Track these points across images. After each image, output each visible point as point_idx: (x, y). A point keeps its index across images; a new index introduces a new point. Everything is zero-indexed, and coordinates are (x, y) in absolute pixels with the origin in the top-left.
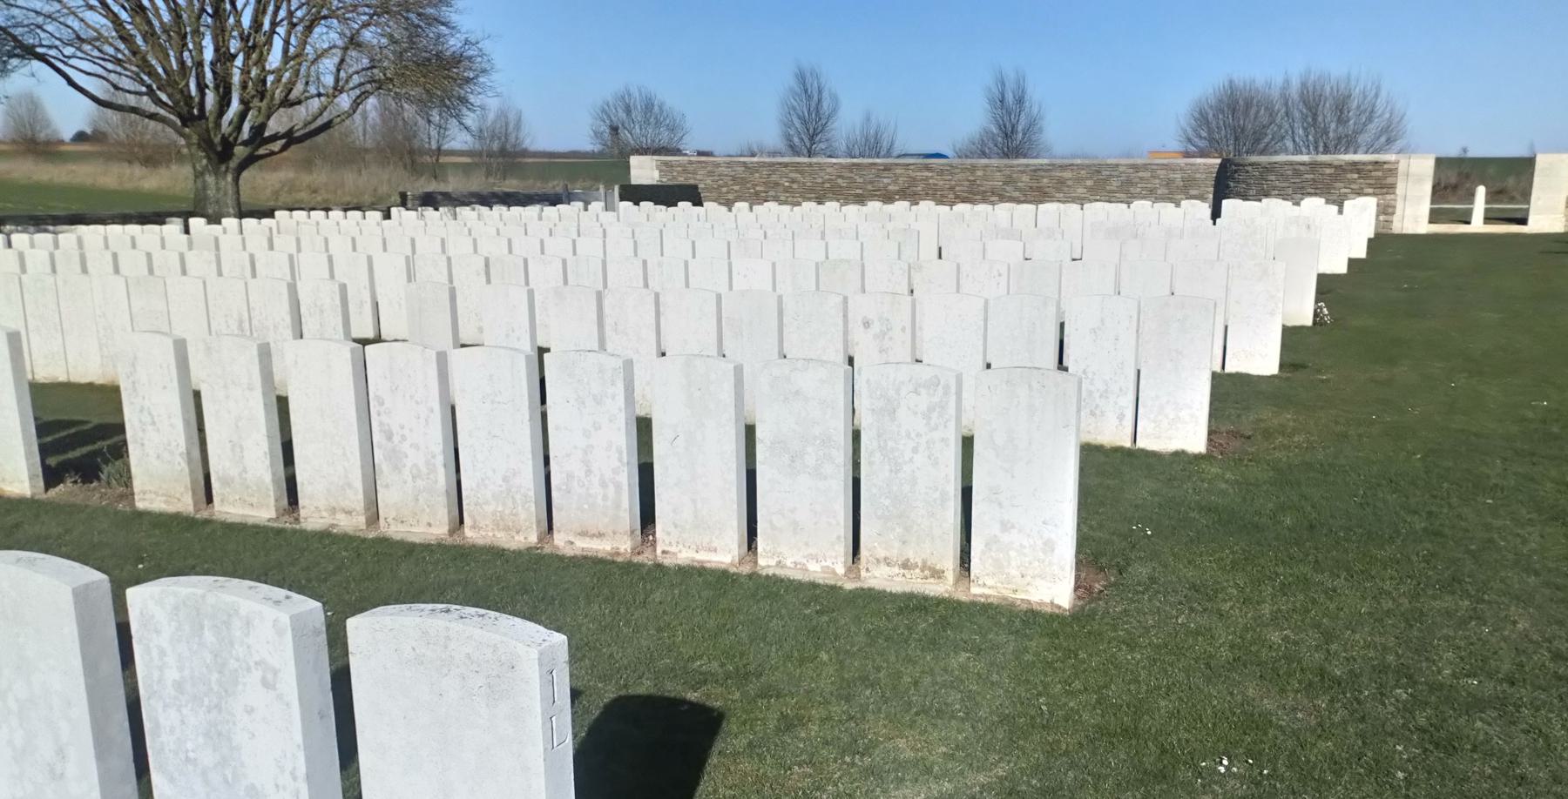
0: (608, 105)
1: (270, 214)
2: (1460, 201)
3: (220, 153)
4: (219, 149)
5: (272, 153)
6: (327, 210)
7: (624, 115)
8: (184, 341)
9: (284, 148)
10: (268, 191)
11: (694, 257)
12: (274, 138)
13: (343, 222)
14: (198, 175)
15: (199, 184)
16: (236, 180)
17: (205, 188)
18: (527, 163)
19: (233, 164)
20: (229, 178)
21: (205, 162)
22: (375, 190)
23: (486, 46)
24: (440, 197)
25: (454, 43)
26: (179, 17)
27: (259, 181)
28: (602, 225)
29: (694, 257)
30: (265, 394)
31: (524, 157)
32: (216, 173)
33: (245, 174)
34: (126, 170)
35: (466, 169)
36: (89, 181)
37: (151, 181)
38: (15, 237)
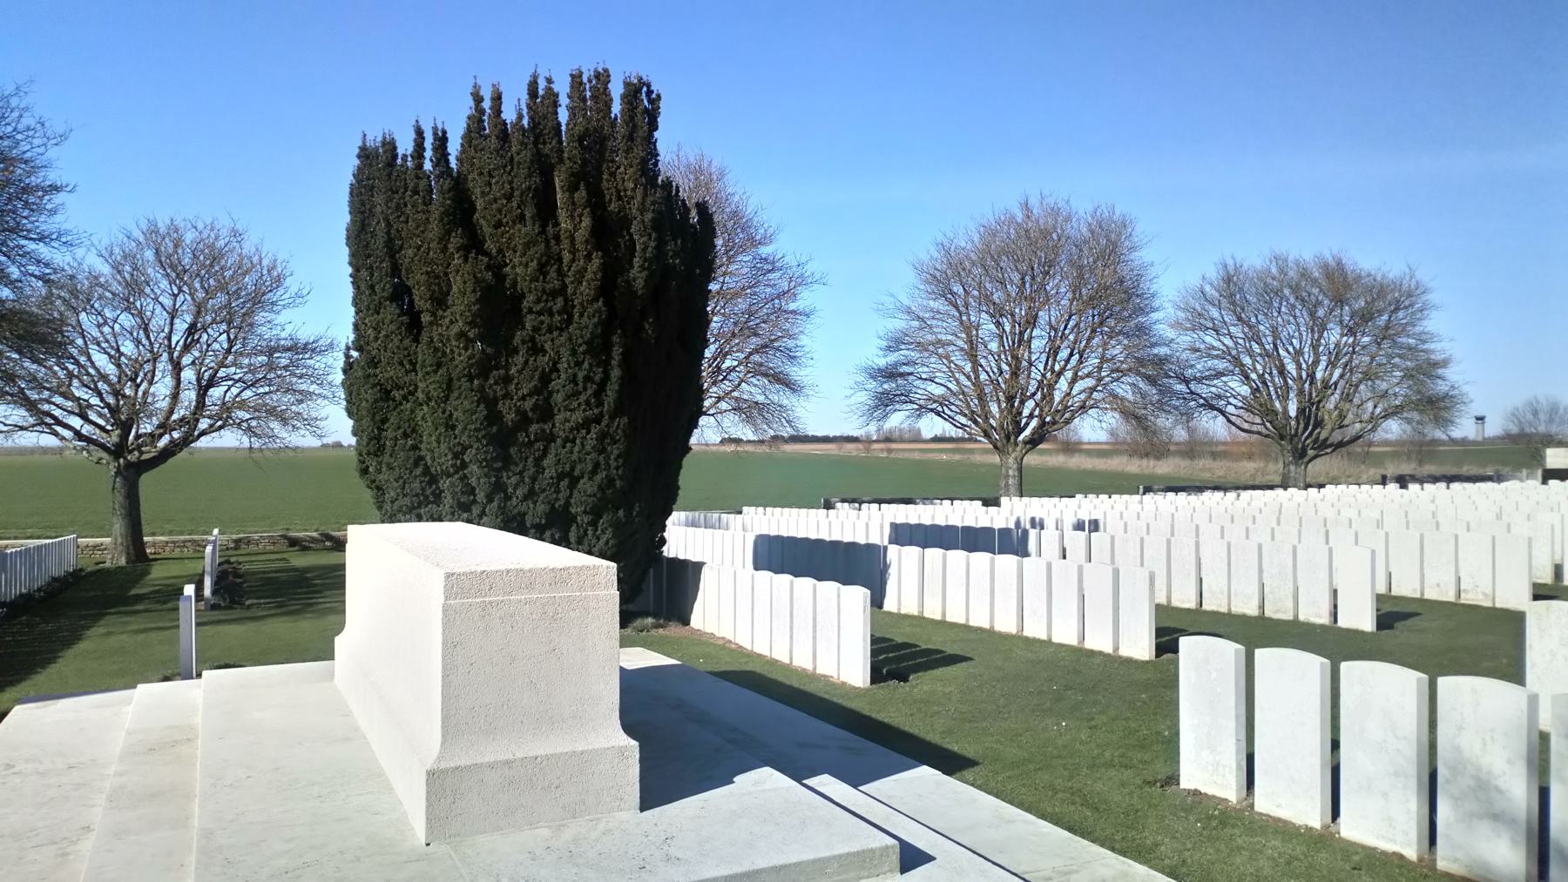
0: (1518, 411)
1: (1321, 486)
2: (1160, 642)
3: (1300, 455)
4: (1300, 451)
5: (1327, 453)
6: (1359, 484)
7: (1531, 417)
8: (1051, 563)
9: (1333, 451)
10: (1248, 475)
11: (1148, 534)
12: (1330, 446)
13: (1371, 491)
14: (1285, 465)
15: (1286, 471)
16: (1306, 468)
17: (1289, 472)
18: (1440, 450)
19: (1306, 460)
20: (1303, 467)
21: (1291, 458)
22: (1327, 474)
23: (1465, 389)
24: (1407, 478)
25: (1442, 387)
26: (982, 390)
27: (1318, 467)
28: (1155, 503)
29: (1148, 534)
30: (1150, 603)
31: (1440, 445)
32: (1296, 464)
33: (1310, 465)
34: (1145, 462)
35: (1395, 455)
36: (1120, 469)
37: (1249, 467)
38: (1013, 498)
